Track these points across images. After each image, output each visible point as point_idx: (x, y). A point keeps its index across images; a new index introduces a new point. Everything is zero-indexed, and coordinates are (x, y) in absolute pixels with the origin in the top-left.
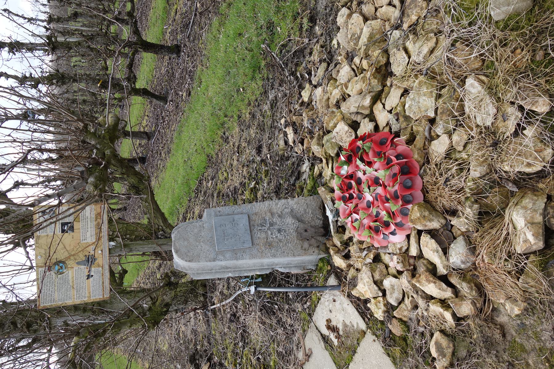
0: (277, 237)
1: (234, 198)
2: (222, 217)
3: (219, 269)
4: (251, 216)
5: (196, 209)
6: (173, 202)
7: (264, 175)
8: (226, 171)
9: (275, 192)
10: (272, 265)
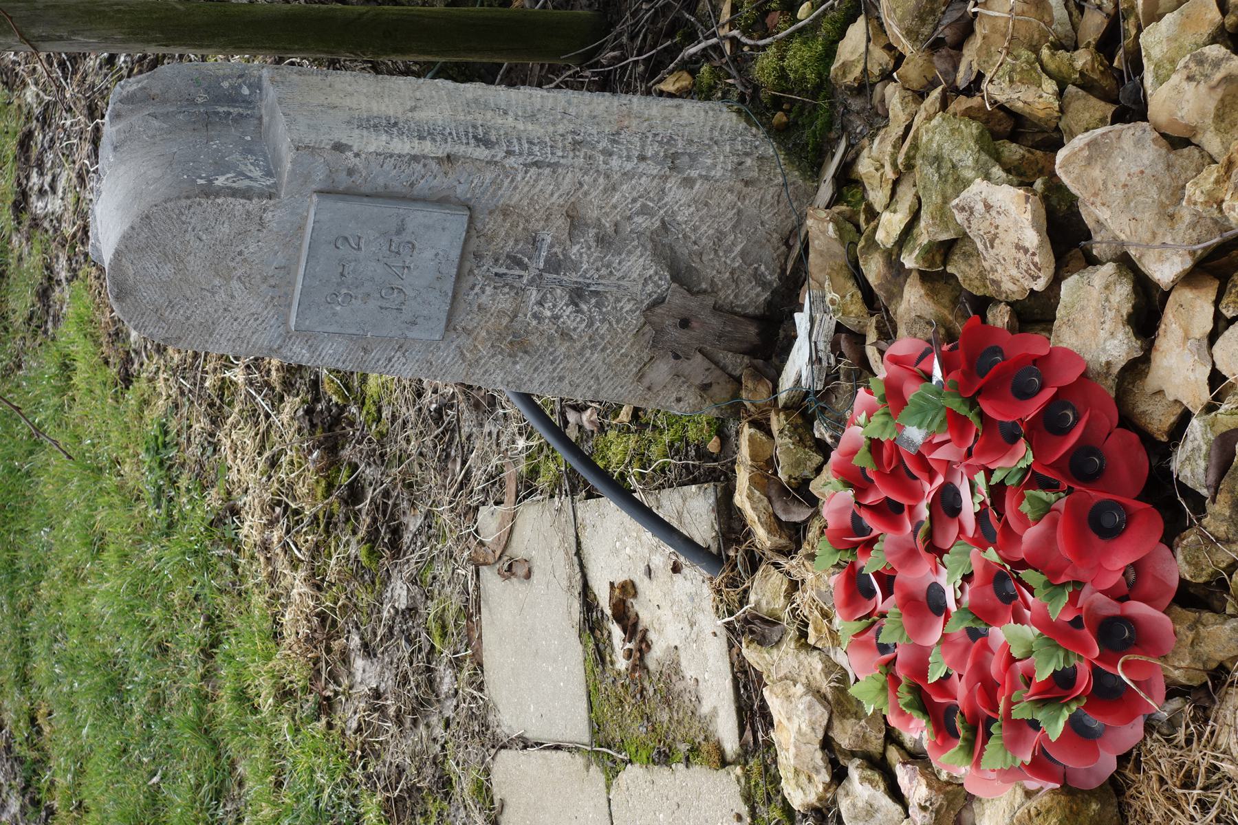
0: (556, 317)
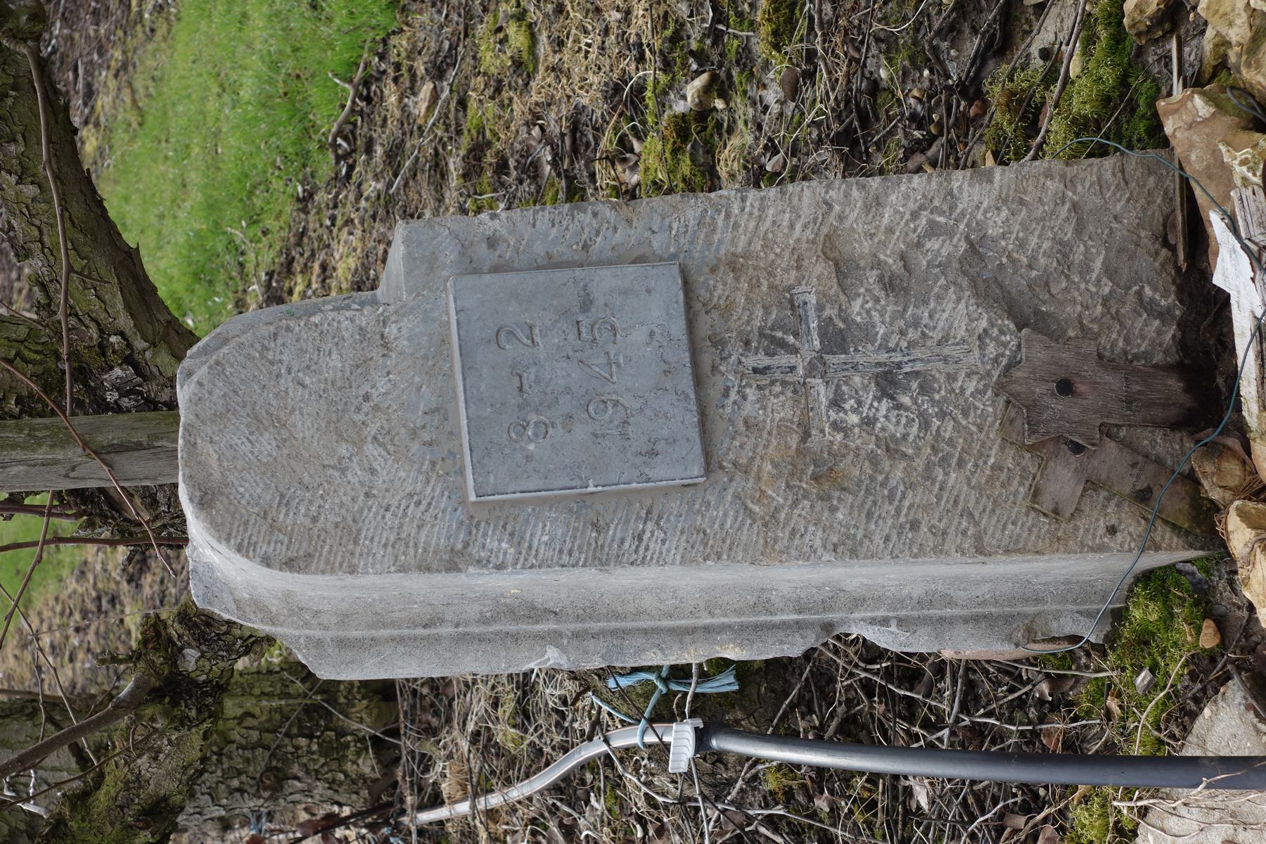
0: (869, 422)
1: (570, 179)
2: (512, 279)
3: (484, 621)
4: (701, 278)
5: (339, 250)
6: (212, 207)
7: (765, 30)
8: (520, 17)
9: (838, 140)
10: (826, 606)
